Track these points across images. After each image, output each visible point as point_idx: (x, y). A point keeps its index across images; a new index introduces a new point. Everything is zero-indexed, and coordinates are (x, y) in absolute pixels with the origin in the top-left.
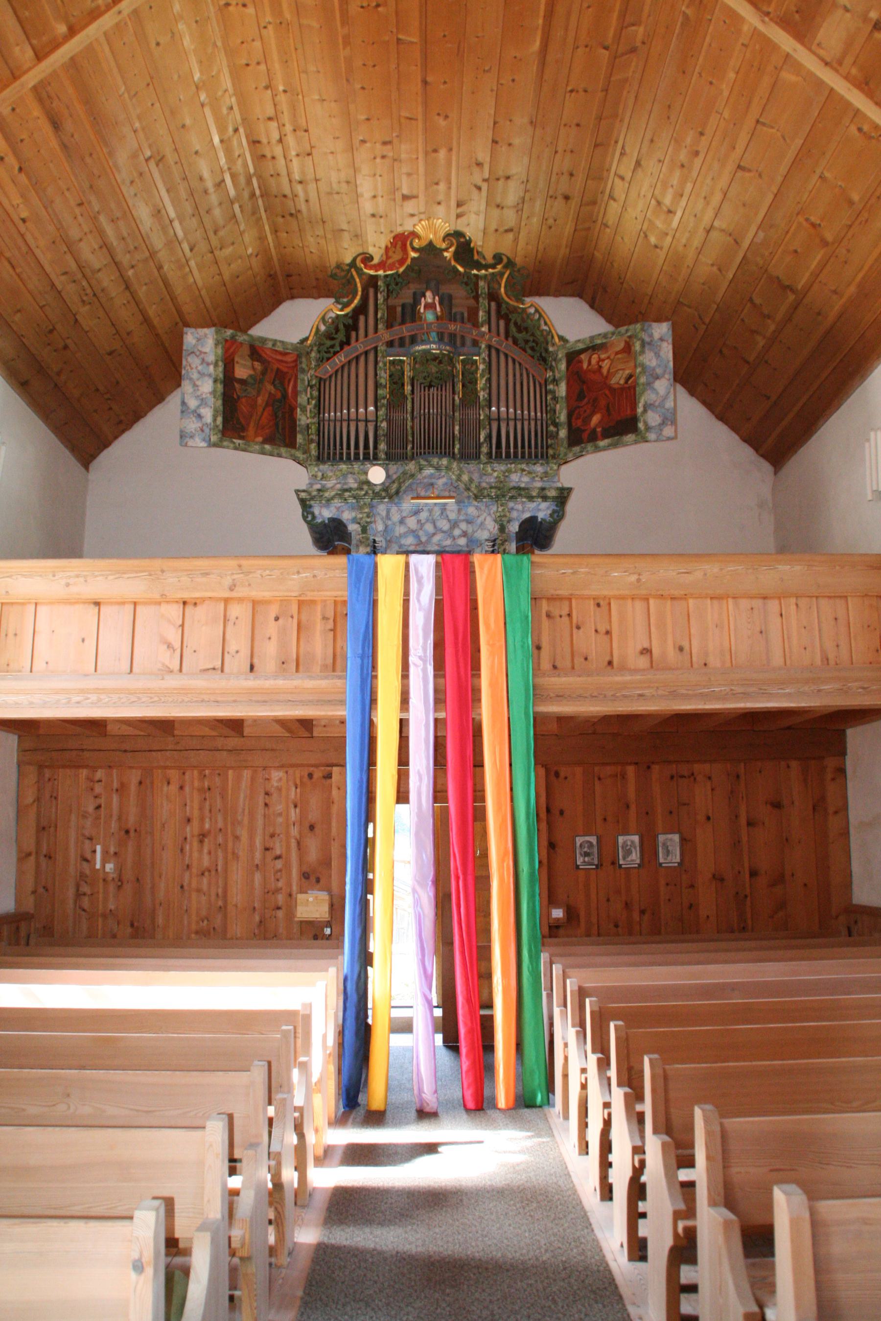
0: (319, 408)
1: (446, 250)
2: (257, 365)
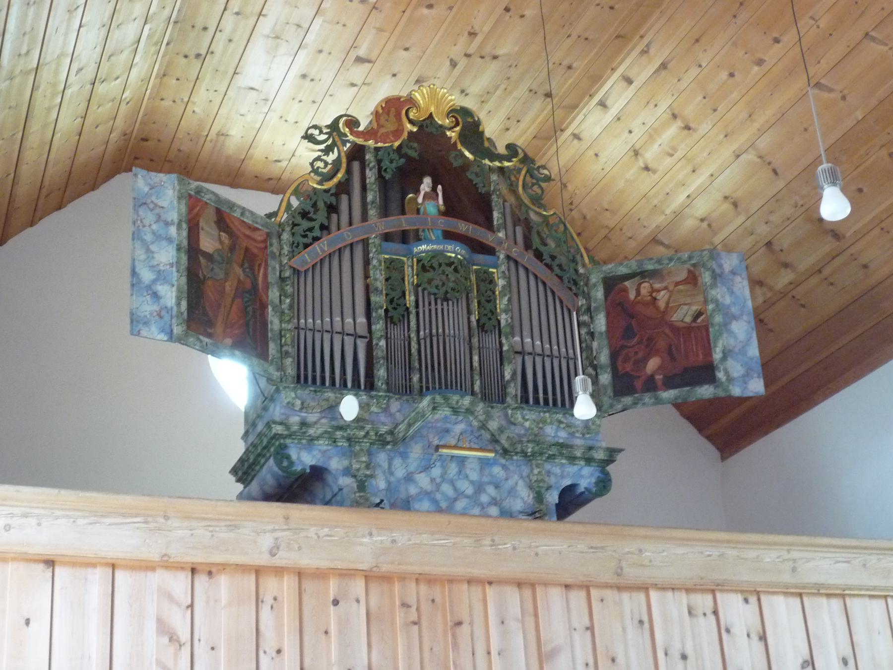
0: (296, 309)
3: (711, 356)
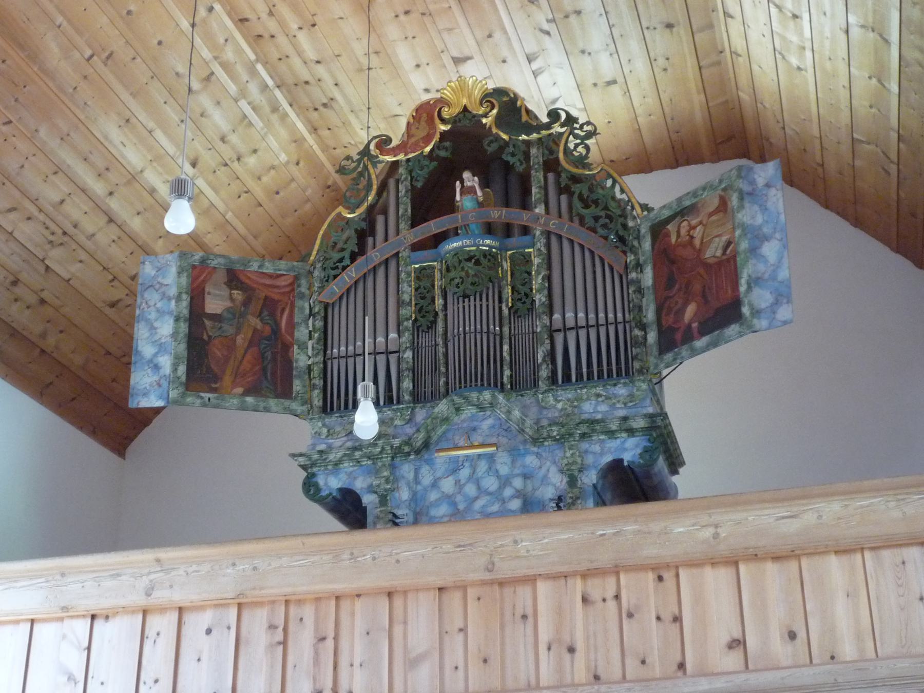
1: (485, 115)
2: (238, 295)
3: (738, 290)
